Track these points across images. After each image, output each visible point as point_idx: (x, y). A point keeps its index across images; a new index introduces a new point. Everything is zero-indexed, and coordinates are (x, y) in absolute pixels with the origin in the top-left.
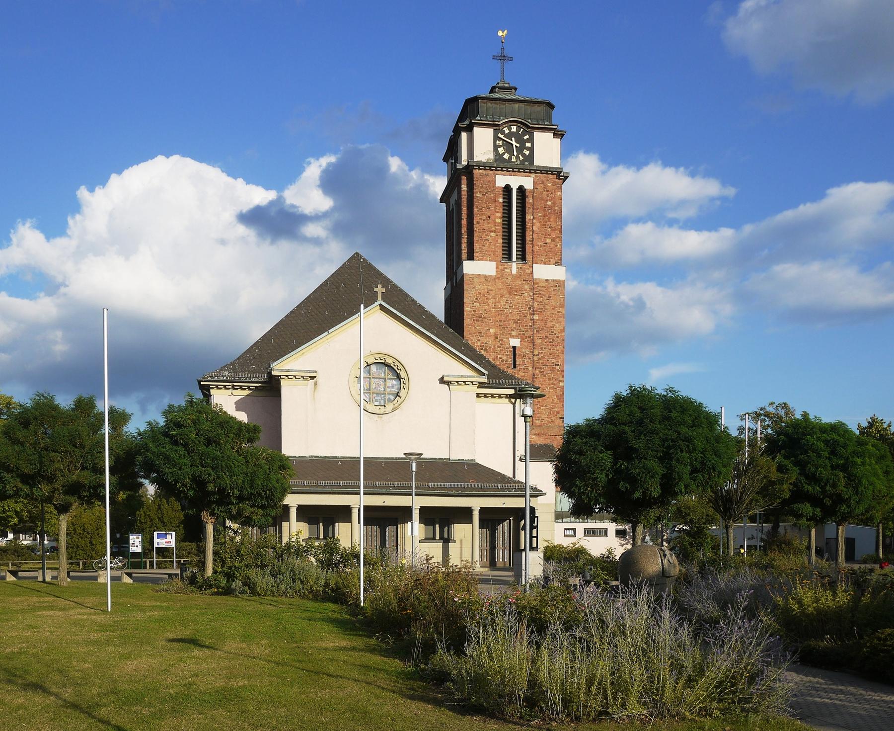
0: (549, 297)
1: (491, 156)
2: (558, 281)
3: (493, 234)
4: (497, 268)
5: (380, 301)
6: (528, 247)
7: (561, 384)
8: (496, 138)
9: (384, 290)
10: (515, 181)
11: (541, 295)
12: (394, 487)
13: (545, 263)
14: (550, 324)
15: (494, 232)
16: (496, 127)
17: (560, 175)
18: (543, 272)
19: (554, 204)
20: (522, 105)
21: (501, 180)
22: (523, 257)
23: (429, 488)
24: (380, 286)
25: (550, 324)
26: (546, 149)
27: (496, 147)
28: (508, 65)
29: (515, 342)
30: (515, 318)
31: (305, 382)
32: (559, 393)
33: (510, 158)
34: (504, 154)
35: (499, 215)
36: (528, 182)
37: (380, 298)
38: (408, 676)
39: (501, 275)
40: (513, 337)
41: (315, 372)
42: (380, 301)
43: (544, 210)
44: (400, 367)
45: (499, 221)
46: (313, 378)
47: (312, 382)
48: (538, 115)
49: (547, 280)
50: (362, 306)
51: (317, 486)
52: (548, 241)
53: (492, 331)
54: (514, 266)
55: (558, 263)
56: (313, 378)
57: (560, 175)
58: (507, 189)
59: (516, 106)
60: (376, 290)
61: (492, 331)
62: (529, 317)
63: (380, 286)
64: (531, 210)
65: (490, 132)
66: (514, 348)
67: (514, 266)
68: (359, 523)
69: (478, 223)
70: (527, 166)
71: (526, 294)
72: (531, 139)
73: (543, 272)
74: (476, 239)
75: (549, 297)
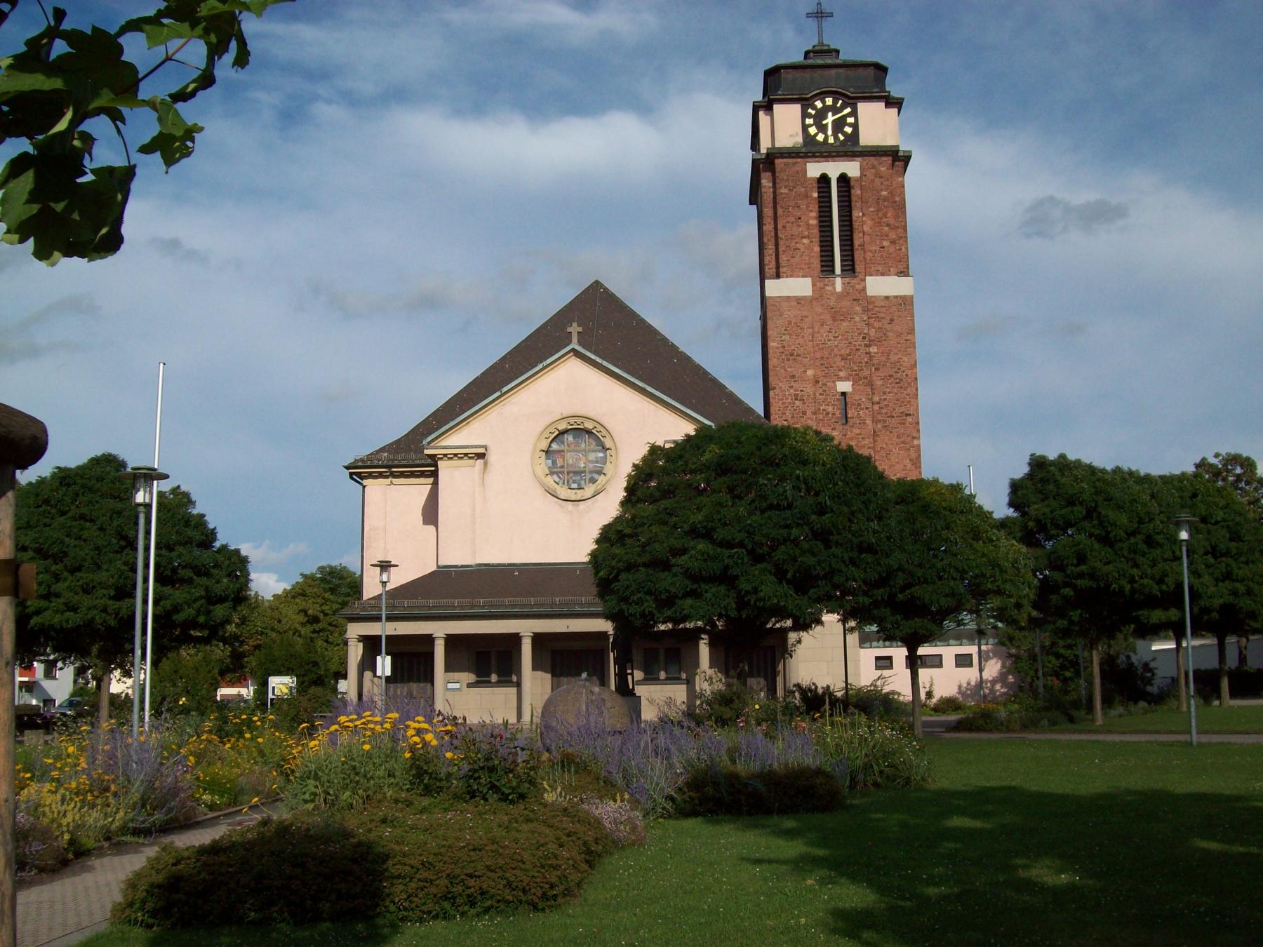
0: (892, 320)
1: (799, 139)
2: (904, 298)
3: (805, 241)
4: (814, 285)
5: (575, 345)
6: (858, 255)
7: (916, 442)
8: (805, 115)
9: (580, 329)
10: (833, 169)
11: (879, 319)
12: (581, 605)
13: (883, 274)
14: (894, 358)
15: (808, 237)
16: (806, 102)
17: (898, 159)
18: (880, 286)
19: (891, 193)
20: (841, 70)
21: (814, 169)
22: (850, 267)
23: (552, 605)
24: (575, 325)
25: (894, 358)
26: (876, 124)
27: (805, 128)
28: (827, 24)
29: (844, 386)
30: (843, 352)
31: (471, 461)
32: (913, 454)
33: (826, 138)
34: (816, 135)
35: (814, 214)
36: (852, 169)
37: (575, 339)
39: (819, 294)
40: (841, 379)
41: (486, 447)
42: (575, 345)
43: (877, 203)
44: (604, 433)
45: (814, 222)
46: (481, 456)
47: (480, 462)
48: (869, 81)
49: (887, 298)
51: (473, 606)
52: (885, 243)
53: (810, 373)
54: (839, 284)
55: (904, 273)
56: (481, 456)
57: (898, 159)
58: (824, 180)
59: (833, 72)
60: (569, 330)
61: (810, 373)
62: (863, 350)
63: (575, 325)
64: (859, 204)
65: (796, 109)
66: (844, 394)
70: (849, 148)
71: (857, 319)
72: (854, 114)
73: (880, 286)
75: (892, 320)
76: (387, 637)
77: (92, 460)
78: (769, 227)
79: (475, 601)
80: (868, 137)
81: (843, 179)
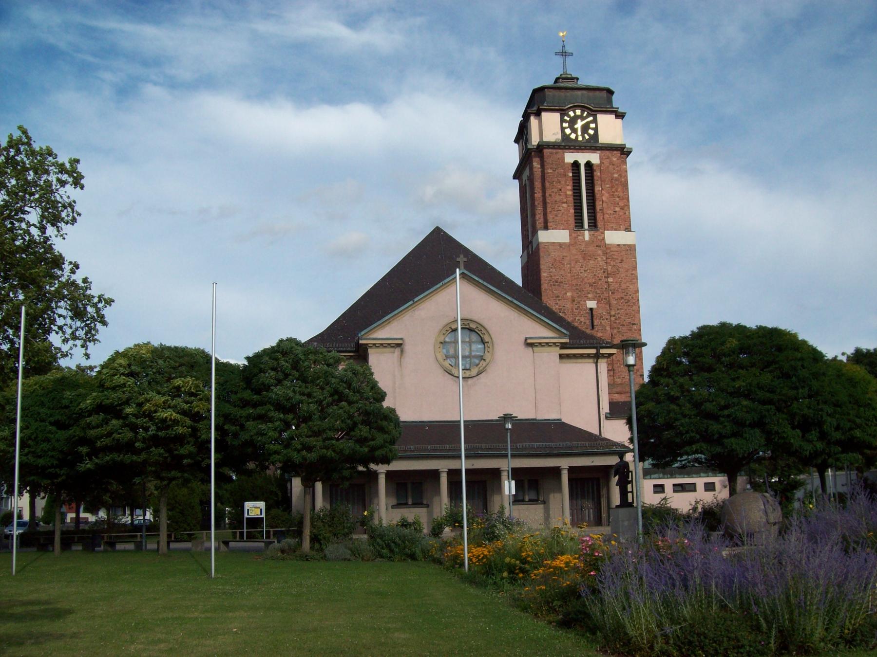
10: (582, 158)
21: (570, 157)
27: (563, 129)
36: (595, 158)
58: (576, 164)
72: (595, 121)
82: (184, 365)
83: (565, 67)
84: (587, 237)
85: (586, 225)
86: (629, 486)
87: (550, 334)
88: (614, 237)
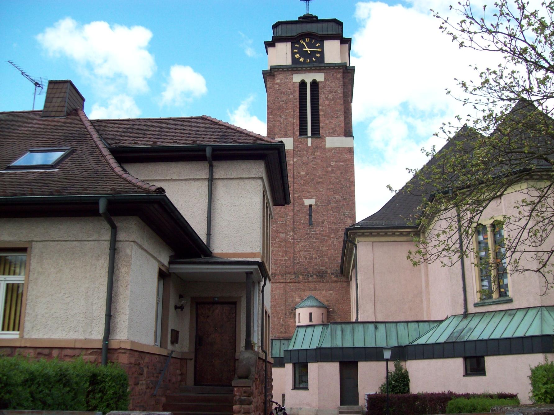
10: (308, 78)
21: (297, 78)
22: (316, 131)
27: (293, 54)
36: (320, 77)
38: (21, 267)
50: (228, 111)
54: (309, 140)
58: (303, 84)
67: (309, 140)
68: (259, 302)
69: (293, 93)
72: (322, 47)
73: (333, 142)
74: (297, 94)
76: (350, 151)
77: (409, 380)
78: (69, 352)
79: (256, 330)
80: (329, 59)
81: (314, 84)
82: (444, 210)
83: (308, 6)
84: (309, 144)
85: (309, 134)
86: (429, 377)
87: (61, 154)
88: (333, 142)
